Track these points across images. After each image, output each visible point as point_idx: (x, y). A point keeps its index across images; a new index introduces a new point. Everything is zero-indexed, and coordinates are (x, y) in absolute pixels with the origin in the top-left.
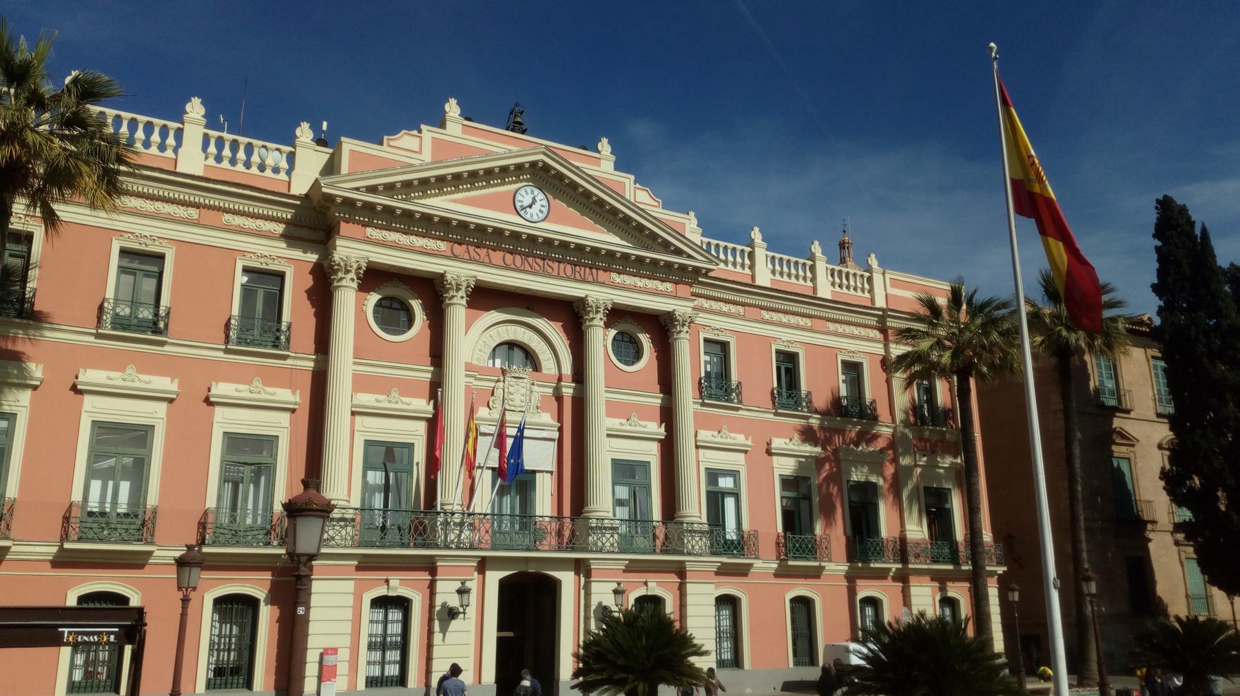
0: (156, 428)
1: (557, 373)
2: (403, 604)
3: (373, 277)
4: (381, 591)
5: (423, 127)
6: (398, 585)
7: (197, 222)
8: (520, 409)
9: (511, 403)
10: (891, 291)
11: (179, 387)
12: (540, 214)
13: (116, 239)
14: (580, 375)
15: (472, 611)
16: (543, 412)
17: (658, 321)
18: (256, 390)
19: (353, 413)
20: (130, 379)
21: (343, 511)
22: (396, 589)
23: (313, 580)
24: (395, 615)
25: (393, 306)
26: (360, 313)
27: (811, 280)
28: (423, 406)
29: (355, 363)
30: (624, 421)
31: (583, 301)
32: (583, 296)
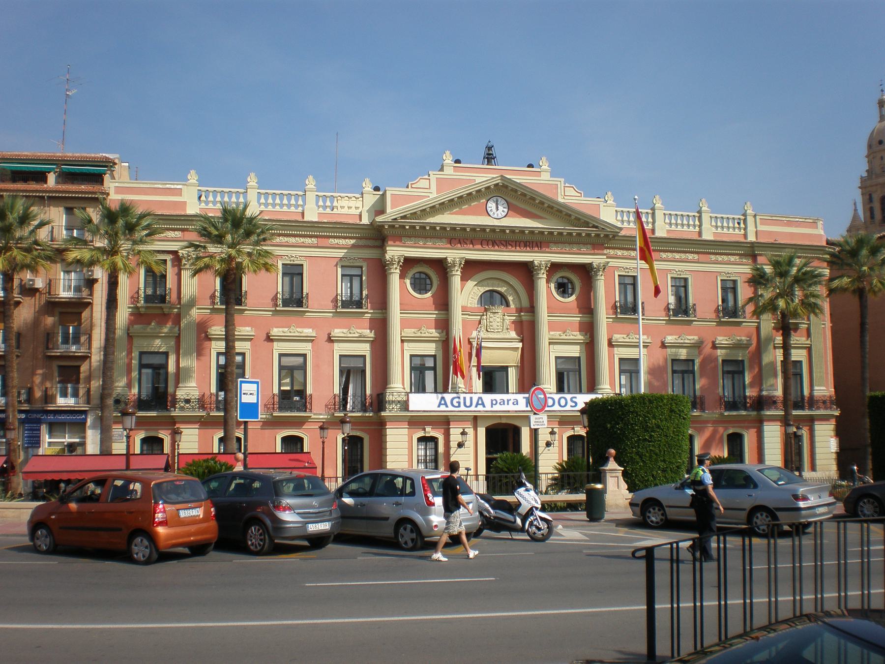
2: (434, 440)
3: (409, 262)
4: (421, 434)
6: (430, 432)
7: (316, 245)
8: (497, 331)
9: (491, 327)
10: (761, 228)
11: (375, 335)
12: (502, 213)
14: (532, 309)
15: (556, 443)
17: (586, 268)
19: (402, 341)
22: (429, 432)
24: (431, 445)
26: (403, 287)
27: (744, 230)
29: (401, 313)
30: (625, 336)
31: (591, 264)
32: (532, 260)
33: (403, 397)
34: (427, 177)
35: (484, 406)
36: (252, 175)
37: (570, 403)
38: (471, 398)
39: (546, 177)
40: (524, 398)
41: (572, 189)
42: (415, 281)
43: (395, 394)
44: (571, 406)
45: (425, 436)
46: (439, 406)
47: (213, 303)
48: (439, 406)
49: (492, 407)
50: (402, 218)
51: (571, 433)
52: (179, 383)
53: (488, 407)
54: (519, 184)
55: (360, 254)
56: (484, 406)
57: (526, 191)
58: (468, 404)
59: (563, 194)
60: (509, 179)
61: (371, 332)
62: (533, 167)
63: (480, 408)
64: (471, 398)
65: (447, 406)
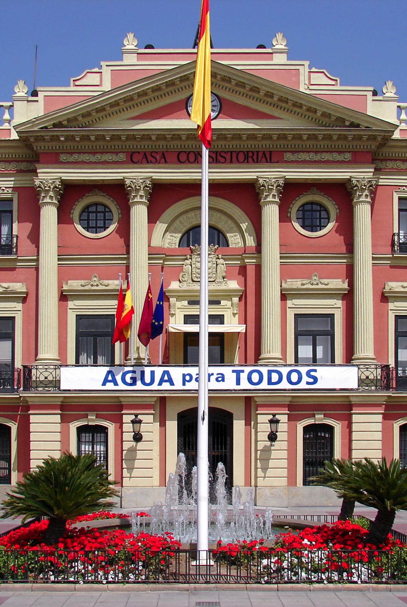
0: (16, 318)
1: (243, 246)
5: (102, 63)
13: (396, 192)
16: (228, 280)
18: (95, 284)
20: (315, 283)
21: (46, 367)
23: (352, 414)
25: (314, 209)
28: (341, 284)
33: (39, 373)
34: (96, 70)
35: (172, 384)
36: (390, 84)
37: (305, 379)
38: (153, 373)
39: (280, 59)
40: (233, 371)
41: (322, 74)
42: (304, 214)
43: (361, 366)
44: (308, 383)
45: (315, 424)
46: (104, 384)
47: (393, 251)
48: (104, 384)
49: (184, 384)
50: (55, 126)
51: (310, 421)
52: (260, 354)
53: (178, 385)
54: (240, 70)
55: (27, 182)
56: (172, 384)
57: (244, 78)
58: (148, 379)
59: (307, 82)
60: (227, 66)
61: (343, 282)
62: (265, 48)
63: (166, 386)
64: (153, 373)
65: (116, 384)
